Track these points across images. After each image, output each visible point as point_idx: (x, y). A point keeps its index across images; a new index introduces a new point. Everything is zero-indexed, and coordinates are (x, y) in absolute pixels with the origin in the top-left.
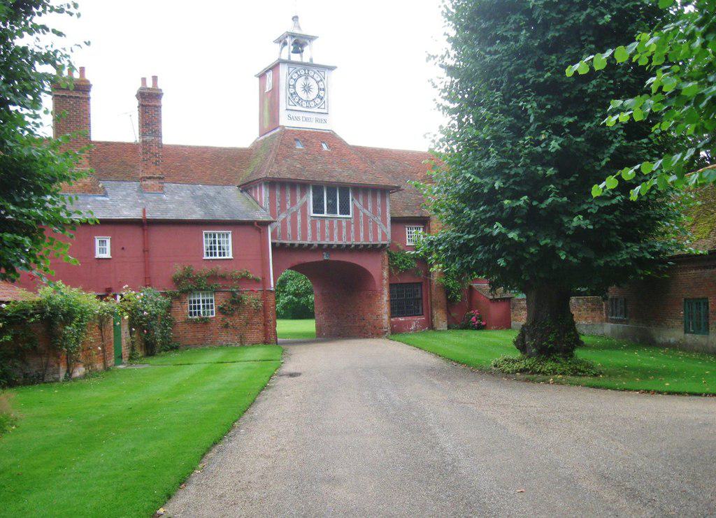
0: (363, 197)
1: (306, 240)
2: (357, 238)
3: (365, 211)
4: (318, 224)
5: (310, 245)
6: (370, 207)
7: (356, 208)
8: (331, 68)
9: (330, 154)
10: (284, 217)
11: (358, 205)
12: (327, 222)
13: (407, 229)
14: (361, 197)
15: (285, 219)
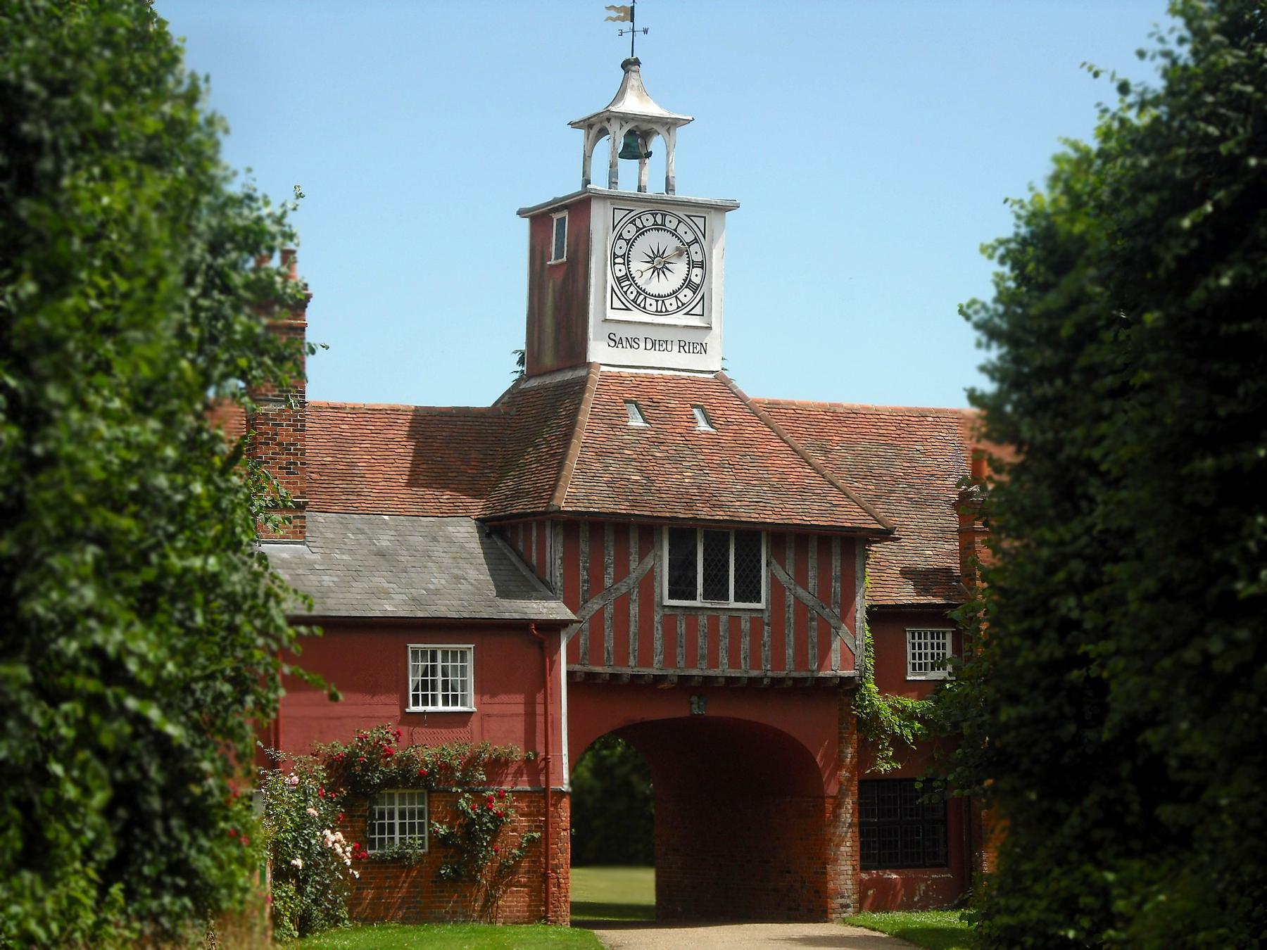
0: (842, 555)
1: (650, 665)
2: (779, 661)
3: (800, 591)
4: (682, 628)
5: (658, 679)
6: (812, 583)
7: (775, 583)
8: (722, 209)
9: (714, 441)
10: (596, 607)
11: (782, 577)
12: (703, 620)
13: (909, 636)
14: (790, 555)
15: (600, 612)
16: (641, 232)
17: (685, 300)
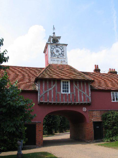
17: (61, 56)
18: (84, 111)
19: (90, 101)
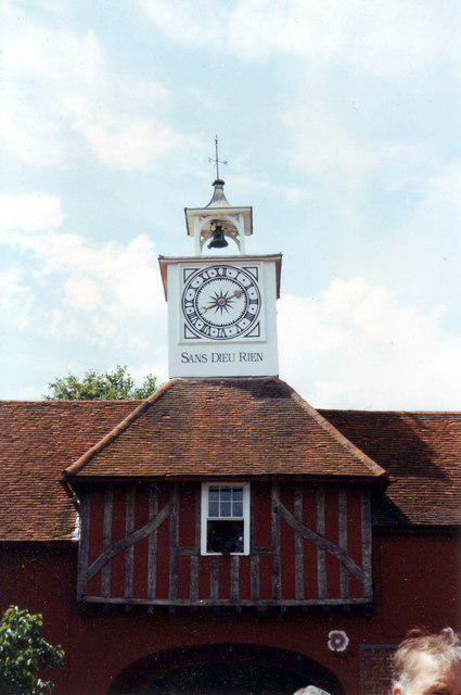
16: (207, 281)
17: (243, 327)
18: (336, 654)
19: (368, 590)
